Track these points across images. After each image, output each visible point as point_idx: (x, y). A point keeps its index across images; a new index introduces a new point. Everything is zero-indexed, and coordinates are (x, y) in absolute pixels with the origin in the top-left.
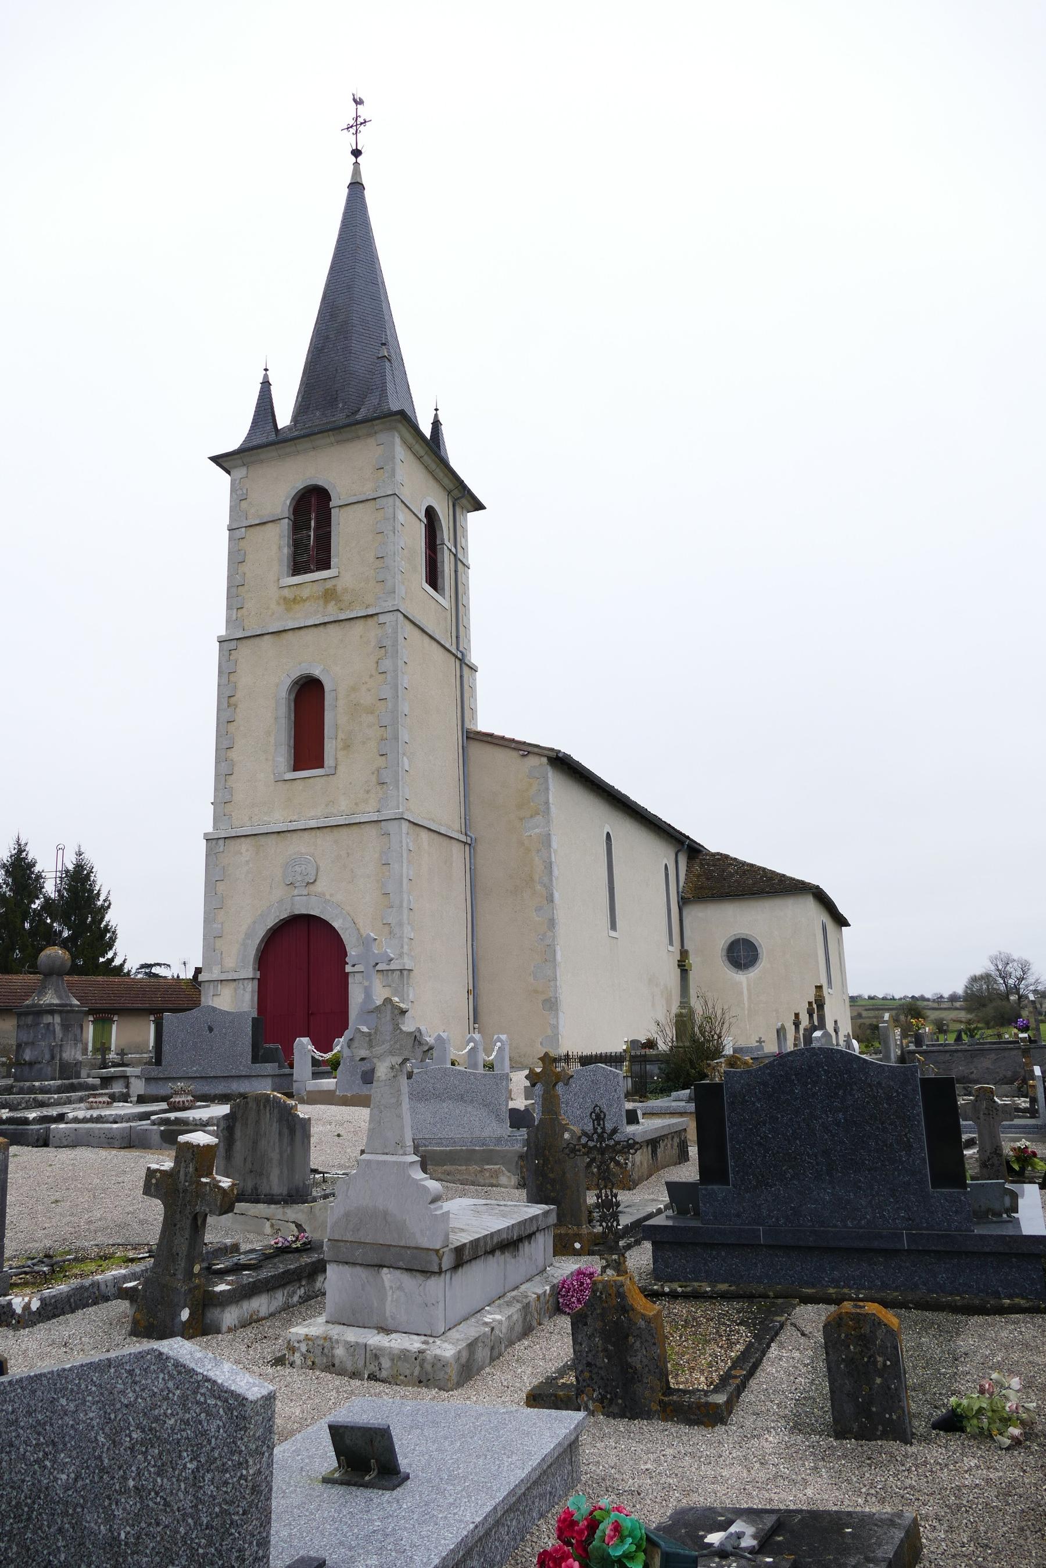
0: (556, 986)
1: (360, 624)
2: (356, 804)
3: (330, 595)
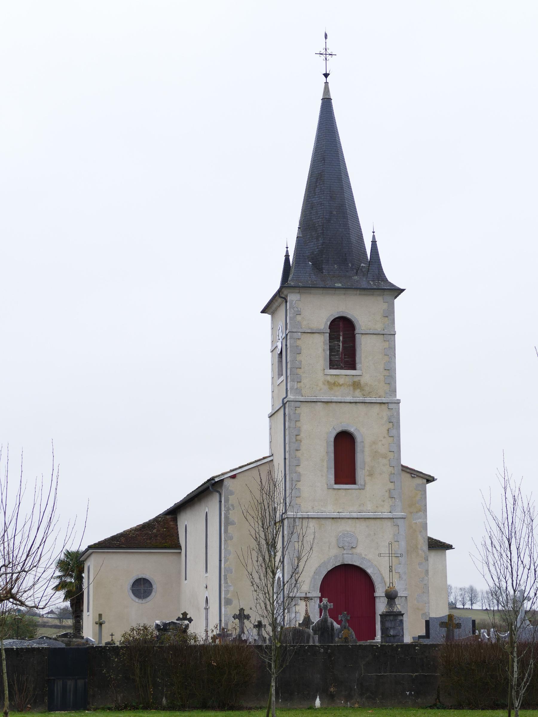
0: (429, 606)
1: (377, 406)
2: (377, 507)
3: (356, 385)
